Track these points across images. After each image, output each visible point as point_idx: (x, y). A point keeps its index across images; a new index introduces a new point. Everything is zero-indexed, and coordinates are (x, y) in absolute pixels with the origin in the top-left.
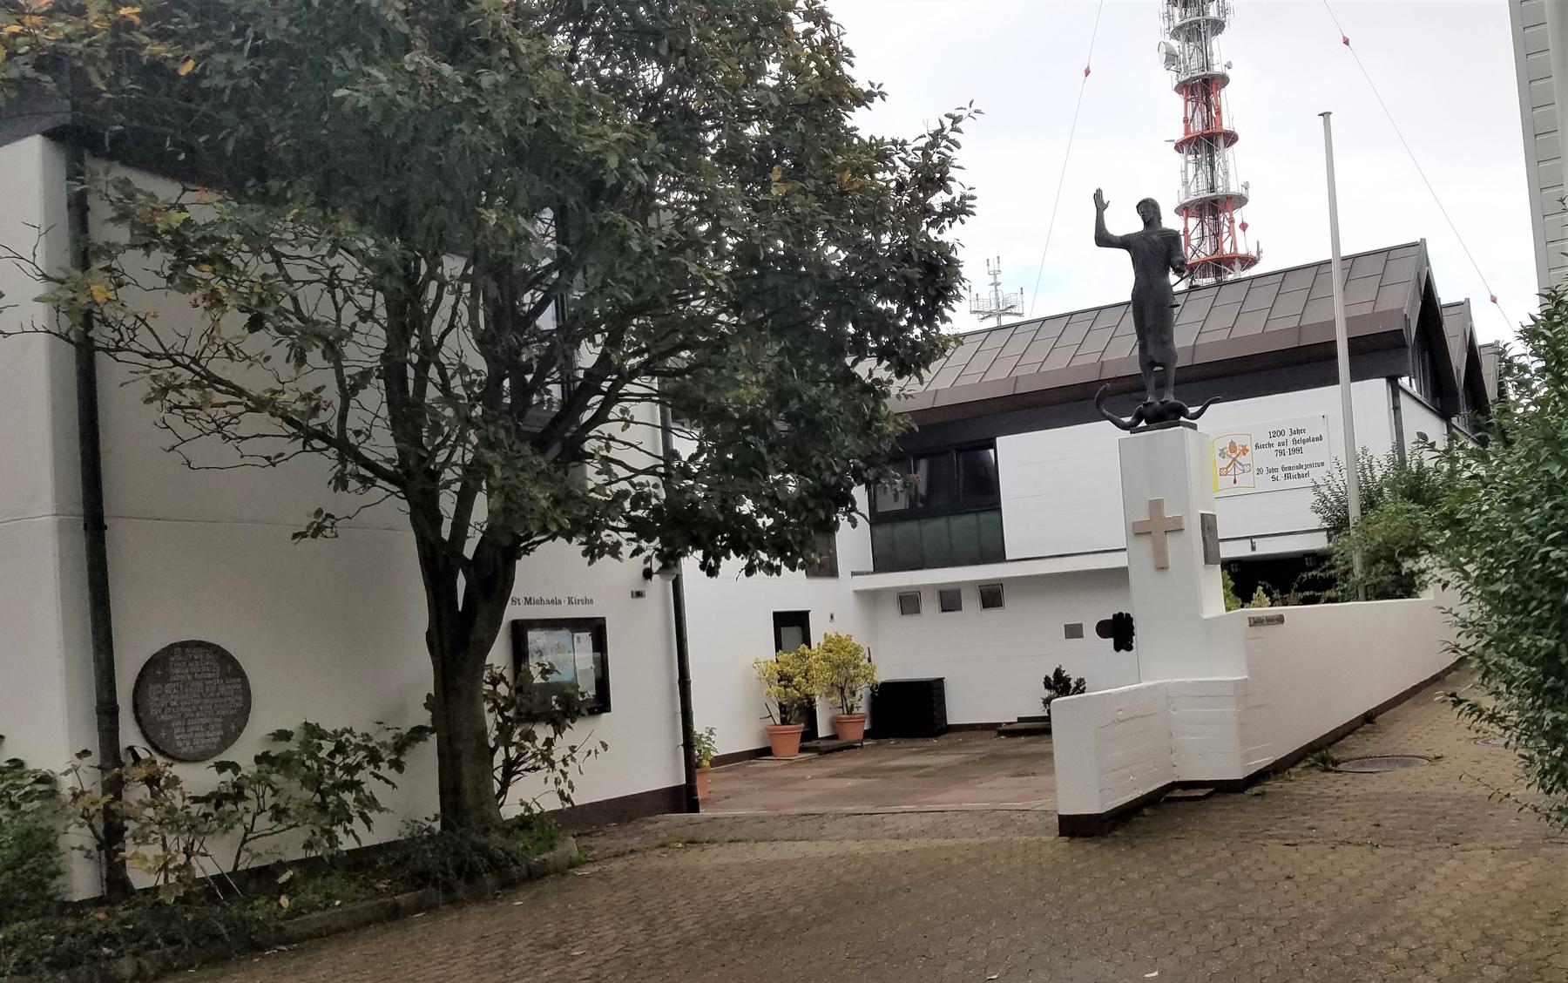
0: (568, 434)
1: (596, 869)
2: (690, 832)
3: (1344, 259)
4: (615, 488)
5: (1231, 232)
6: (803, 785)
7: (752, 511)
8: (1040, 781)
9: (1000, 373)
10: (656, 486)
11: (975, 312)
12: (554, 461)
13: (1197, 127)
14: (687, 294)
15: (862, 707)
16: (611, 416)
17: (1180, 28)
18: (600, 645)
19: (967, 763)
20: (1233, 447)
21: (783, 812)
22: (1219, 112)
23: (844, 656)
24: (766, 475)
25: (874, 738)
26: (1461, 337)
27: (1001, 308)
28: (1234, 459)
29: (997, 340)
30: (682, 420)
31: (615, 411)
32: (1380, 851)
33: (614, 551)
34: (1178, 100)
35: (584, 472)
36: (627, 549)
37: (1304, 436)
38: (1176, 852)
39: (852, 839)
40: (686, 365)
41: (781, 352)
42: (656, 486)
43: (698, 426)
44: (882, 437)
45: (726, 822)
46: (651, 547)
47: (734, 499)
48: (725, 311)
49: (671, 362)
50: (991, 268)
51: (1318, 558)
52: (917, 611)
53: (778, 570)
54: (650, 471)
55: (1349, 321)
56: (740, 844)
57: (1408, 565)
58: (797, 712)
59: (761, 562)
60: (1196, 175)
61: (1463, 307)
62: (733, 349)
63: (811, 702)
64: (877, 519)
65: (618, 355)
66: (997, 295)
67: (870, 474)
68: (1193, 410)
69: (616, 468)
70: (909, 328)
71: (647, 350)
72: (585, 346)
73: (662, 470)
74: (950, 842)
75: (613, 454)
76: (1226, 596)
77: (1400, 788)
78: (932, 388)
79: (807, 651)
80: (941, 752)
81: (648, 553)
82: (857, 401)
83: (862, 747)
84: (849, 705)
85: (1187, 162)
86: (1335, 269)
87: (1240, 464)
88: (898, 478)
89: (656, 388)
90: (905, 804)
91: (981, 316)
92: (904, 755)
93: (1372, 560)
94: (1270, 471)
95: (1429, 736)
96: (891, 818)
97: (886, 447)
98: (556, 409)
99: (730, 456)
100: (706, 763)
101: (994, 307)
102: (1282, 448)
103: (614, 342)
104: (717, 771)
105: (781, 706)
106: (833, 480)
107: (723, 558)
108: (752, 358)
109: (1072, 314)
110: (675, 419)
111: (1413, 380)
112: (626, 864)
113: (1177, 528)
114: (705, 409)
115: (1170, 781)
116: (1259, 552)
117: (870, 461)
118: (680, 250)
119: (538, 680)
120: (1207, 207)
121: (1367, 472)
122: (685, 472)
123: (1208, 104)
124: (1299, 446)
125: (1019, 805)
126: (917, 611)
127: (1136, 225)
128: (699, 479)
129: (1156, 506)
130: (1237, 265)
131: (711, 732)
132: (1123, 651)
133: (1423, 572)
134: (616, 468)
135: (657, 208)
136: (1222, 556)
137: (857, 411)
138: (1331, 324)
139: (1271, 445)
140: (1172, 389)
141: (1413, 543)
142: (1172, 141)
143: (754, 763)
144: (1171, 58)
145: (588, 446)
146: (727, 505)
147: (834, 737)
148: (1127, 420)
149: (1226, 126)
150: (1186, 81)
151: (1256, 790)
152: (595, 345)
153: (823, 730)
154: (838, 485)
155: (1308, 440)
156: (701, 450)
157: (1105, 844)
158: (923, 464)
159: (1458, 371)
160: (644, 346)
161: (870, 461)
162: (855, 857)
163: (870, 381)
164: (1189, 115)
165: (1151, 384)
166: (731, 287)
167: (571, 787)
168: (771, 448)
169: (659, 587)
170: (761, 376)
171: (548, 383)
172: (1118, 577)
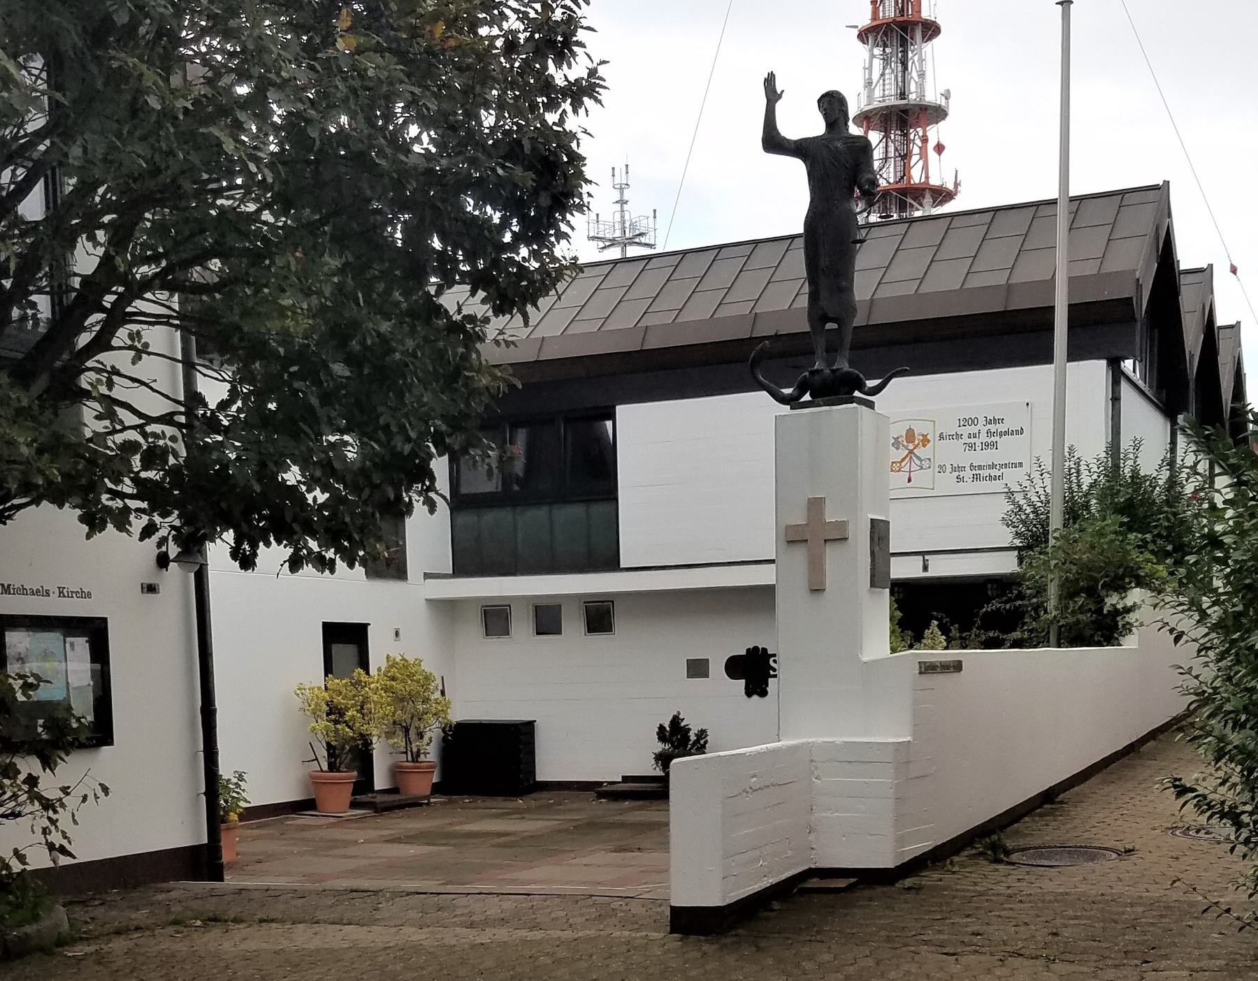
0: (58, 364)
1: (92, 948)
2: (211, 906)
3: (1073, 199)
4: (119, 438)
5: (923, 154)
6: (351, 851)
7: (299, 482)
8: (648, 858)
9: (626, 320)
10: (173, 439)
11: (593, 238)
12: (39, 397)
14: (218, 180)
15: (431, 754)
16: (115, 342)
18: (100, 653)
19: (560, 831)
20: (910, 435)
21: (329, 884)
23: (412, 686)
24: (319, 435)
25: (444, 793)
26: (1198, 314)
27: (627, 235)
28: (911, 452)
29: (624, 275)
30: (211, 356)
31: (122, 336)
32: (1057, 967)
33: (121, 520)
35: (79, 414)
36: (138, 523)
37: (1002, 428)
38: (810, 958)
39: (413, 925)
40: (217, 280)
41: (342, 271)
42: (173, 439)
43: (230, 362)
44: (473, 392)
45: (256, 895)
46: (168, 523)
47: (276, 463)
48: (267, 206)
49: (196, 273)
50: (617, 180)
51: (1000, 584)
52: (506, 632)
53: (331, 566)
54: (167, 419)
55: (1072, 281)
56: (274, 925)
57: (1112, 600)
58: (350, 756)
59: (310, 551)
60: (883, 75)
61: (1205, 274)
62: (279, 262)
63: (367, 744)
64: (459, 502)
65: (125, 260)
66: (622, 217)
67: (456, 441)
68: (871, 383)
69: (122, 413)
70: (513, 247)
71: (164, 255)
72: (83, 243)
73: (182, 419)
74: (537, 935)
75: (117, 393)
76: (892, 632)
77: (1083, 888)
78: (538, 334)
79: (364, 678)
80: (527, 816)
81: (163, 532)
82: (441, 344)
83: (428, 804)
84: (415, 750)
85: (873, 56)
86: (1062, 211)
87: (918, 458)
88: (492, 449)
89: (176, 307)
90: (480, 881)
91: (601, 245)
92: (482, 817)
93: (1069, 591)
94: (954, 469)
95: (1119, 822)
96: (463, 901)
97: (477, 407)
98: (42, 329)
99: (272, 406)
100: (233, 817)
101: (618, 234)
102: (972, 440)
103: (120, 237)
104: (250, 827)
105: (329, 746)
106: (407, 448)
107: (261, 544)
108: (304, 274)
109: (721, 247)
110: (201, 352)
111: (1137, 362)
112: (130, 944)
113: (839, 537)
114: (241, 339)
115: (806, 868)
116: (932, 573)
117: (456, 424)
118: (210, 120)
119: (20, 697)
120: (894, 119)
121: (1074, 479)
122: (212, 424)
124: (993, 439)
125: (621, 890)
126: (506, 632)
127: (815, 126)
128: (230, 435)
129: (816, 505)
130: (928, 199)
131: (241, 778)
132: (755, 697)
133: (1128, 610)
134: (122, 413)
135: (185, 59)
136: (892, 577)
137: (441, 355)
138: (1049, 285)
139: (959, 436)
140: (847, 353)
141: (1121, 571)
142: (856, 27)
143: (293, 819)
145: (85, 381)
146: (267, 469)
147: (394, 791)
148: (787, 391)
149: (925, 14)
151: (908, 882)
152: (96, 244)
153: (380, 781)
154: (414, 454)
155: (1006, 433)
156: (234, 395)
157: (724, 946)
158: (522, 435)
159: (1192, 356)
160: (161, 250)
161: (456, 424)
162: (417, 948)
163: (459, 317)
165: (820, 344)
166: (277, 174)
167: (65, 836)
168: (326, 399)
169: (176, 578)
170: (314, 300)
171: (32, 293)
172: (762, 597)
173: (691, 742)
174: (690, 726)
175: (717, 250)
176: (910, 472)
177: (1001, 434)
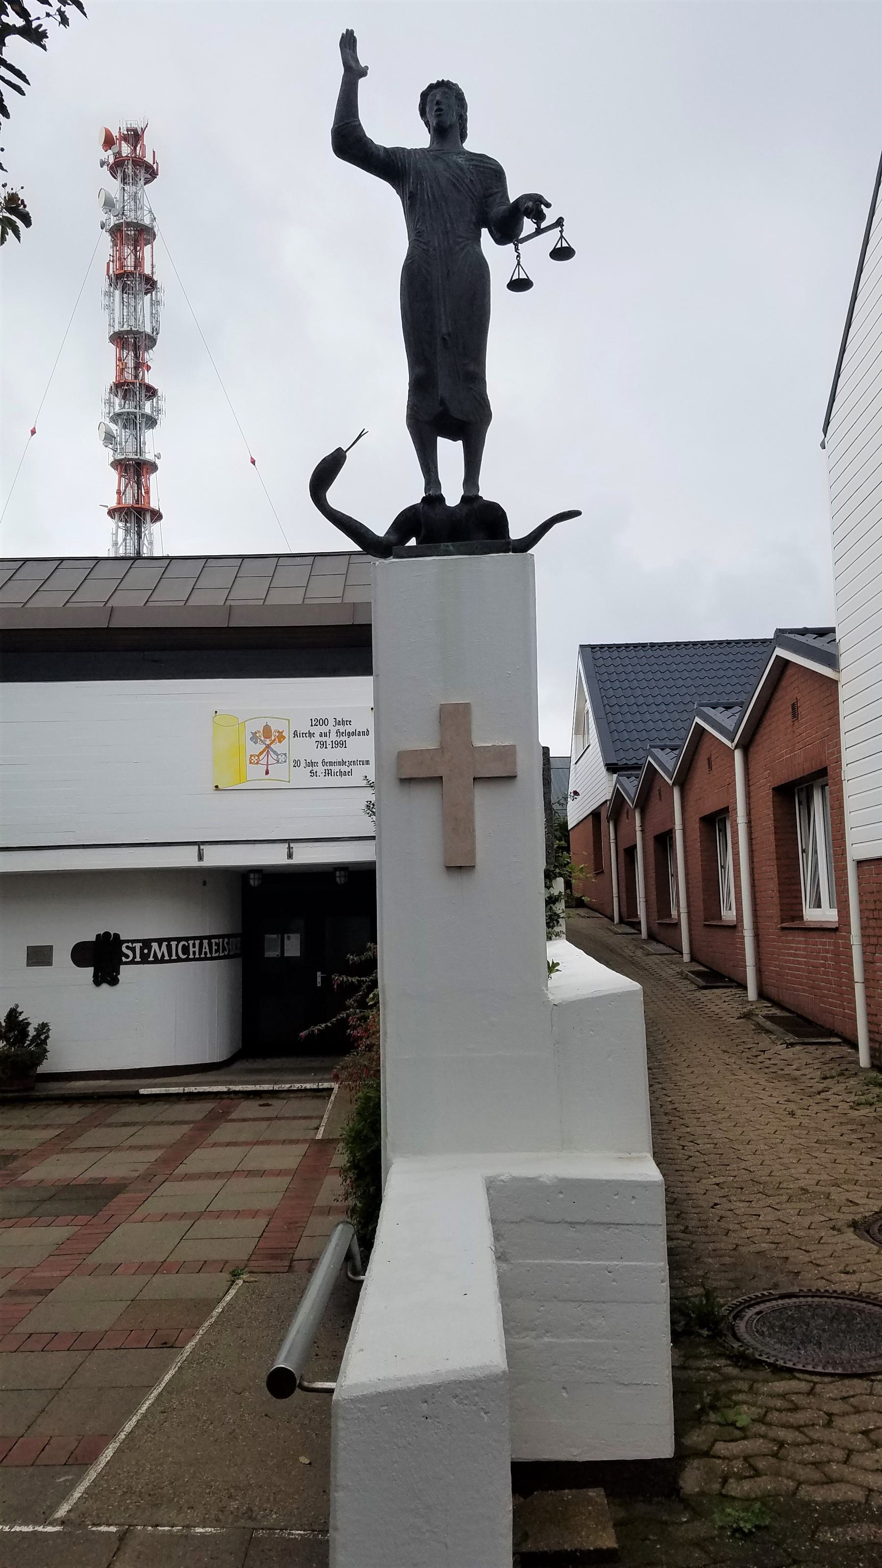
13: (129, 500)
17: (119, 415)
20: (267, 731)
22: (147, 492)
28: (268, 746)
34: (114, 475)
37: (349, 729)
60: (125, 540)
85: (118, 527)
102: (324, 739)
123: (139, 483)
132: (105, 986)
139: (311, 735)
142: (107, 507)
144: (109, 438)
149: (154, 505)
150: (121, 460)
155: (353, 734)
164: (122, 489)
173: (30, 1038)
174: (29, 1020)
175: (60, 561)
176: (267, 765)
177: (349, 734)
